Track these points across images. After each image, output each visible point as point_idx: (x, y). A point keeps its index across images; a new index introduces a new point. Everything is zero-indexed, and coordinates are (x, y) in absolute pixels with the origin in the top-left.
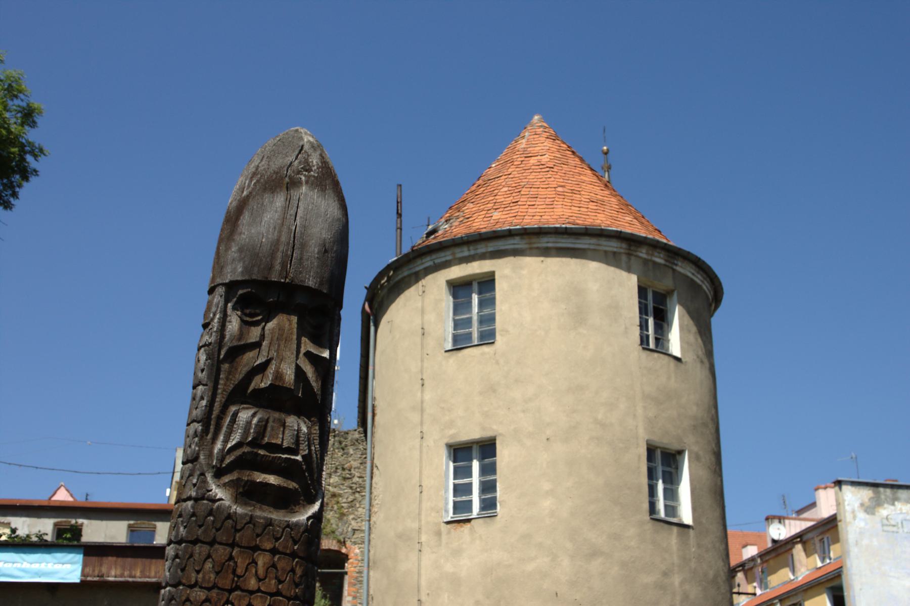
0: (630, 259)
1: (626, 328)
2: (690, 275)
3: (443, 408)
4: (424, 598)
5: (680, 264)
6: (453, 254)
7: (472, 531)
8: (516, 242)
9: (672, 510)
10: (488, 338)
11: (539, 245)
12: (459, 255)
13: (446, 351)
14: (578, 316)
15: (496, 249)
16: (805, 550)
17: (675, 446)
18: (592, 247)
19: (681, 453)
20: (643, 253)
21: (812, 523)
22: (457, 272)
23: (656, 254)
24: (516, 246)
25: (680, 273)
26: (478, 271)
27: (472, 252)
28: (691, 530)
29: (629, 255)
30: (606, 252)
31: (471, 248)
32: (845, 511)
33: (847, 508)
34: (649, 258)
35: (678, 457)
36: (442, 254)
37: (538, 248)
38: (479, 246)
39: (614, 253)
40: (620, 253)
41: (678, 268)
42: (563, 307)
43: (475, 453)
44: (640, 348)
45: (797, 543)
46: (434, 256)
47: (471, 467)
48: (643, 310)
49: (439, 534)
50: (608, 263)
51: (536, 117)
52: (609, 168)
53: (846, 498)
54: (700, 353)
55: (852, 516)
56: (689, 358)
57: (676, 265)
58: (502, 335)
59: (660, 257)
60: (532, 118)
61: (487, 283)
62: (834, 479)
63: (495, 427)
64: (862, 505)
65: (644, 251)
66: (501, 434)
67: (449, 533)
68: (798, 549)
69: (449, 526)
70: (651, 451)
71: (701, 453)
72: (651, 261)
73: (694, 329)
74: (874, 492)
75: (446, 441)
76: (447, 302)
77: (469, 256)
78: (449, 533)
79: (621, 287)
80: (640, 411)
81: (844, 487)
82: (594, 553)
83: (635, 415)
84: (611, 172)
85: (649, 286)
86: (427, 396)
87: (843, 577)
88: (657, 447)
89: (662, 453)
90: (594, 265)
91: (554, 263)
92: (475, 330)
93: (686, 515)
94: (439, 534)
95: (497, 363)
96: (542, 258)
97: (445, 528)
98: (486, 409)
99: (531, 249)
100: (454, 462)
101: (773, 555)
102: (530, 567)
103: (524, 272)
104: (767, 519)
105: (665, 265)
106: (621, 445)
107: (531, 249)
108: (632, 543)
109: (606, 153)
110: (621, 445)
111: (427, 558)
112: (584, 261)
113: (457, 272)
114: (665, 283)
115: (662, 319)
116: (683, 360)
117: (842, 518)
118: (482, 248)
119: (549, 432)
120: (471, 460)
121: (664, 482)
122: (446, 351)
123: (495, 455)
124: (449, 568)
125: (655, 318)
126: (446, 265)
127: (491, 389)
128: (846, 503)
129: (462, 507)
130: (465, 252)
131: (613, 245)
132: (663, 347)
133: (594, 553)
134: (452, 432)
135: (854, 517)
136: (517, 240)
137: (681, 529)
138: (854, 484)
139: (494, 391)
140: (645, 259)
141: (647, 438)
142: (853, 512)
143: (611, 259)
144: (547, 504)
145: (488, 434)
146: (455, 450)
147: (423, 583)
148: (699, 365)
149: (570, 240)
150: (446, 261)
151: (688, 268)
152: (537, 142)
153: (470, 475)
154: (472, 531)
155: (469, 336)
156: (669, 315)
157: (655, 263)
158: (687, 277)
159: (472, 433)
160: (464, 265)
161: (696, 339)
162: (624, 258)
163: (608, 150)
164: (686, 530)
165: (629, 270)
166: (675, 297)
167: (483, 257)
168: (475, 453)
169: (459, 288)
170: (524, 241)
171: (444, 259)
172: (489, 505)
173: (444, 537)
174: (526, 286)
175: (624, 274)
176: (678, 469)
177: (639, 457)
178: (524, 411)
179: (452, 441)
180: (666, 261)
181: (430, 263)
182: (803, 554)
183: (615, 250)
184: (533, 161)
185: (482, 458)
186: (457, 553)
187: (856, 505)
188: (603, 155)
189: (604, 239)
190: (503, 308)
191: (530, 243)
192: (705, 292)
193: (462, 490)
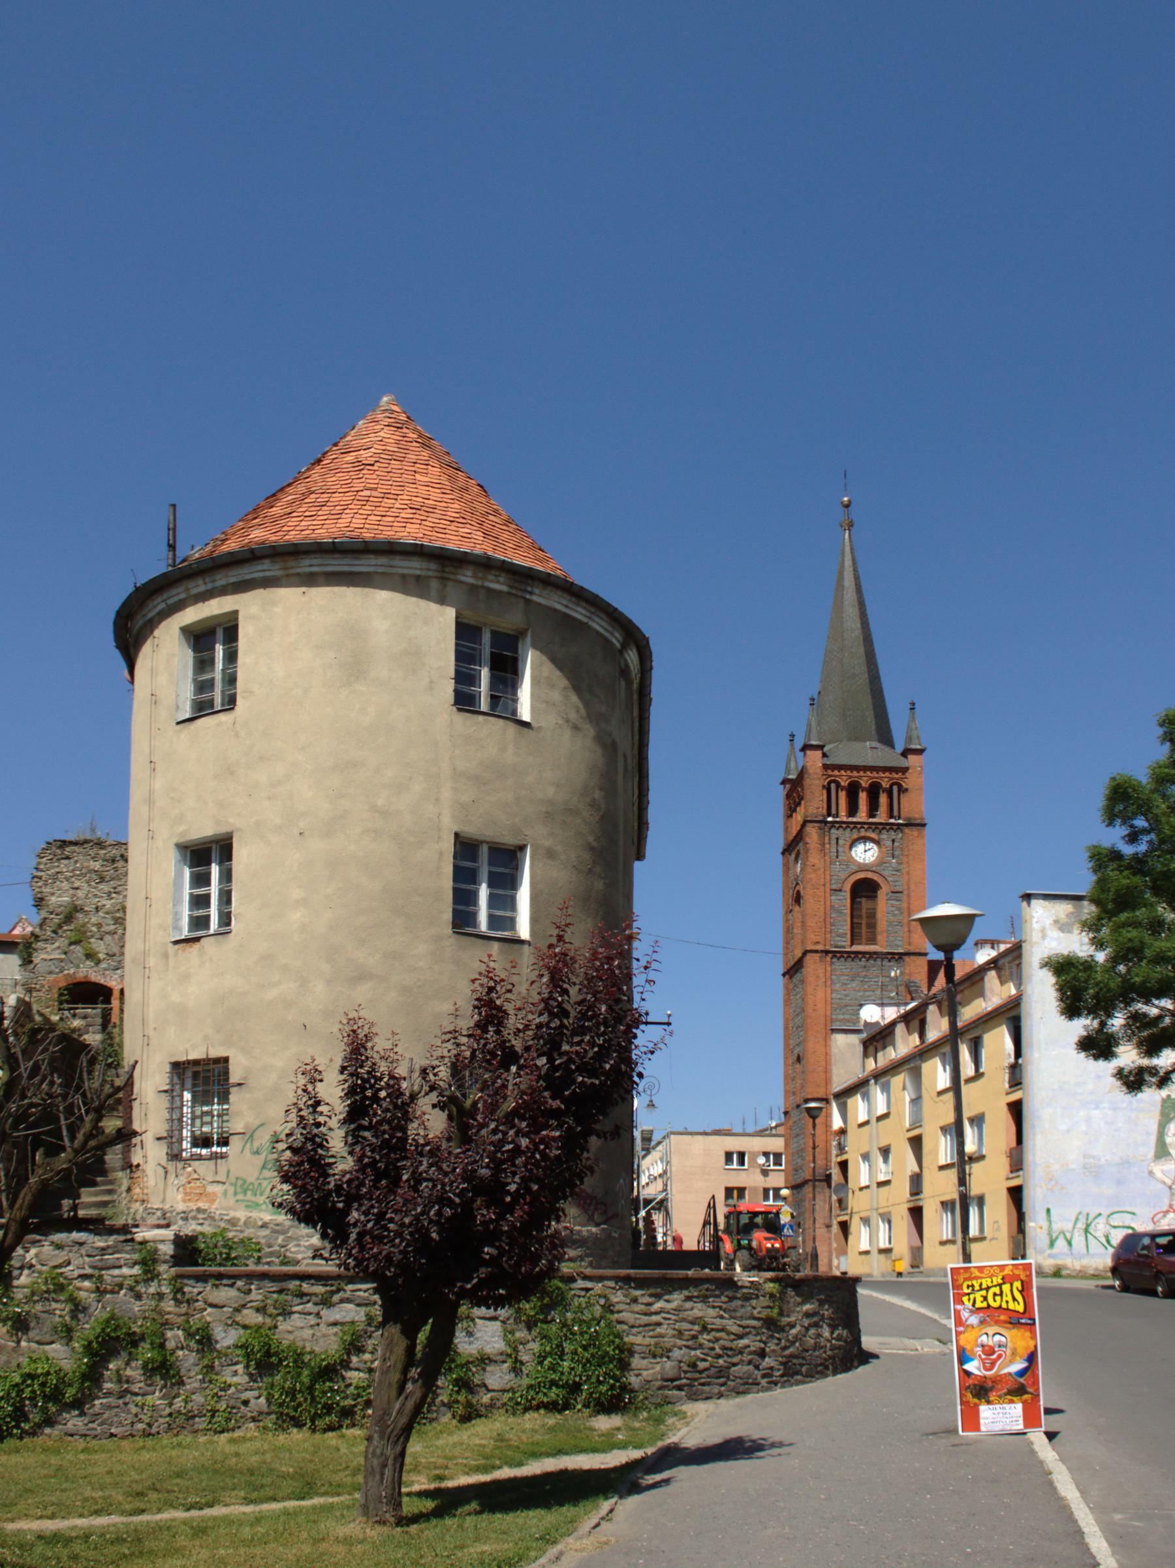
0: (445, 586)
1: (431, 682)
2: (559, 607)
3: (172, 798)
4: (151, 1033)
5: (537, 591)
6: (188, 590)
7: (202, 952)
8: (265, 567)
9: (503, 920)
10: (231, 702)
11: (298, 570)
12: (195, 591)
13: (178, 723)
14: (355, 668)
15: (240, 578)
16: (999, 977)
17: (509, 840)
18: (380, 570)
19: (522, 848)
20: (468, 576)
21: (1009, 946)
22: (192, 615)
23: (491, 577)
24: (268, 574)
25: (539, 604)
26: (217, 612)
27: (210, 586)
28: (526, 946)
29: (443, 580)
30: (403, 576)
31: (207, 580)
32: (1032, 929)
33: (1035, 926)
34: (480, 583)
35: (519, 854)
36: (174, 591)
37: (298, 574)
38: (218, 577)
39: (418, 577)
40: (428, 577)
41: (534, 598)
42: (332, 655)
43: (207, 854)
44: (454, 708)
45: (990, 969)
46: (165, 596)
47: (209, 874)
48: (465, 658)
49: (166, 956)
50: (406, 591)
51: (385, 399)
52: (851, 525)
53: (1035, 914)
54: (573, 716)
55: (1040, 935)
56: (549, 721)
57: (531, 593)
58: (244, 698)
59: (498, 582)
60: (380, 398)
61: (229, 629)
62: (1022, 893)
63: (231, 820)
64: (1056, 922)
65: (469, 573)
66: (238, 829)
67: (176, 954)
68: (991, 977)
69: (177, 947)
70: (466, 847)
71: (559, 849)
72: (483, 587)
73: (562, 682)
74: (1075, 907)
75: (175, 840)
76: (186, 656)
77: (207, 591)
78: (176, 954)
79: (428, 628)
80: (446, 794)
81: (1034, 902)
82: (361, 976)
83: (437, 800)
84: (853, 529)
85: (485, 625)
86: (158, 784)
87: (1023, 1005)
88: (482, 842)
89: (490, 848)
90: (383, 596)
91: (321, 595)
92: (218, 697)
93: (524, 929)
94: (166, 956)
95: (237, 735)
96: (304, 589)
97: (172, 949)
98: (221, 797)
99: (288, 576)
100: (190, 867)
101: (967, 984)
102: (271, 994)
103: (278, 610)
104: (976, 944)
105: (509, 593)
106: (412, 839)
107: (288, 576)
108: (421, 964)
109: (847, 506)
110: (412, 839)
111: (155, 986)
112: (367, 590)
113: (192, 615)
114: (511, 620)
115: (506, 671)
116: (534, 725)
117: (1028, 938)
118: (221, 579)
119: (302, 825)
120: (210, 864)
121: (490, 886)
122: (178, 723)
123: (230, 859)
124: (176, 997)
125: (492, 669)
126: (180, 606)
127: (229, 771)
128: (1034, 920)
129: (199, 923)
130: (199, 586)
131: (414, 566)
132: (506, 709)
133: (361, 976)
134: (182, 828)
135: (1044, 937)
136: (266, 564)
137: (506, 946)
138: (1047, 897)
139: (232, 773)
140: (472, 585)
141: (455, 829)
142: (1043, 930)
143: (413, 586)
144: (296, 916)
145: (223, 829)
146: (193, 852)
147: (151, 1016)
148: (568, 733)
149: (345, 561)
150: (180, 601)
151: (556, 598)
152: (375, 434)
153: (208, 884)
154: (202, 952)
155: (211, 703)
156: (520, 663)
157: (489, 590)
158: (556, 610)
159: (204, 829)
160: (200, 605)
161: (566, 697)
162: (434, 584)
163: (850, 501)
164: (516, 946)
165: (442, 601)
166: (529, 639)
167: (223, 591)
168: (207, 854)
169: (201, 639)
170: (277, 566)
171: (176, 599)
172: (226, 919)
173: (171, 961)
174: (281, 627)
175: (434, 607)
176: (517, 868)
177: (441, 854)
178: (269, 798)
179: (182, 840)
180: (510, 586)
181: (162, 606)
182: (997, 981)
183: (418, 572)
184: (349, 458)
185: (220, 864)
186: (185, 978)
187: (1048, 922)
188: (842, 509)
189: (398, 558)
190: (247, 661)
191: (286, 569)
192: (598, 632)
193: (200, 901)
